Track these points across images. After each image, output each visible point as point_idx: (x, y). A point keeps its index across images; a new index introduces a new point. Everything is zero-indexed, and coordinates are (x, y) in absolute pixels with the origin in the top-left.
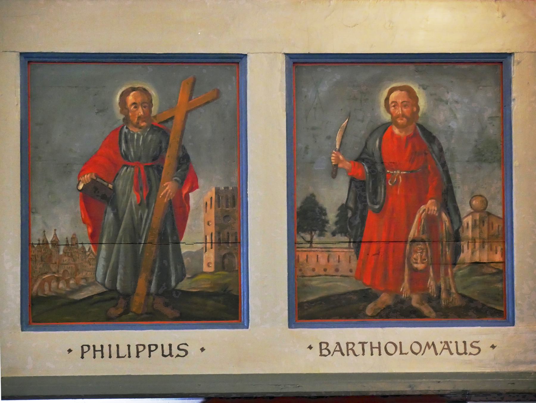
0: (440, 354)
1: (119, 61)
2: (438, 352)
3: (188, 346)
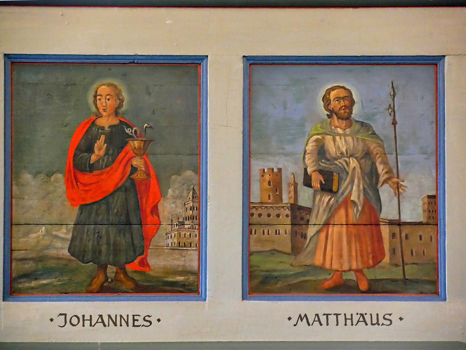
0: (312, 325)
1: (370, 63)
2: (353, 323)
3: (140, 316)
